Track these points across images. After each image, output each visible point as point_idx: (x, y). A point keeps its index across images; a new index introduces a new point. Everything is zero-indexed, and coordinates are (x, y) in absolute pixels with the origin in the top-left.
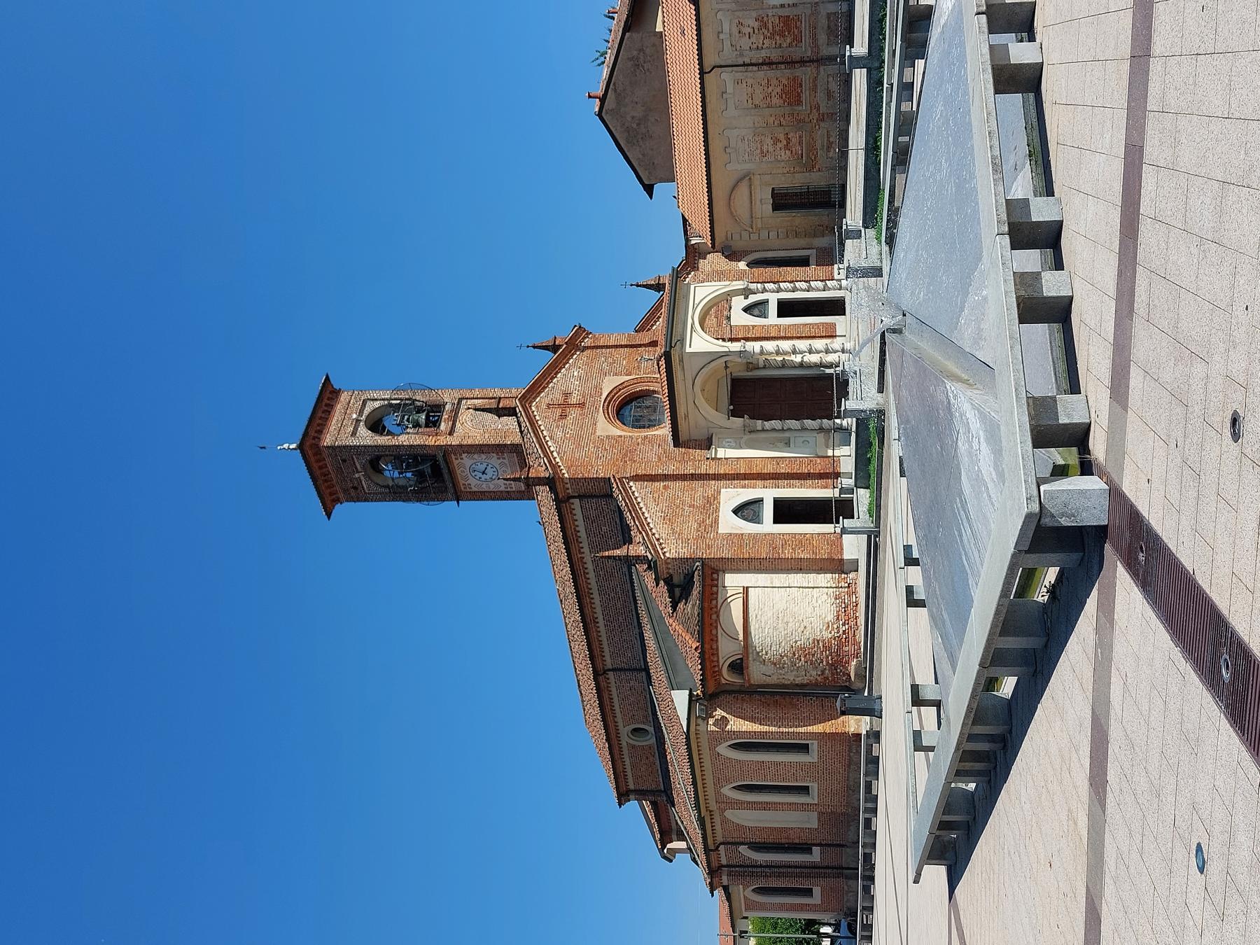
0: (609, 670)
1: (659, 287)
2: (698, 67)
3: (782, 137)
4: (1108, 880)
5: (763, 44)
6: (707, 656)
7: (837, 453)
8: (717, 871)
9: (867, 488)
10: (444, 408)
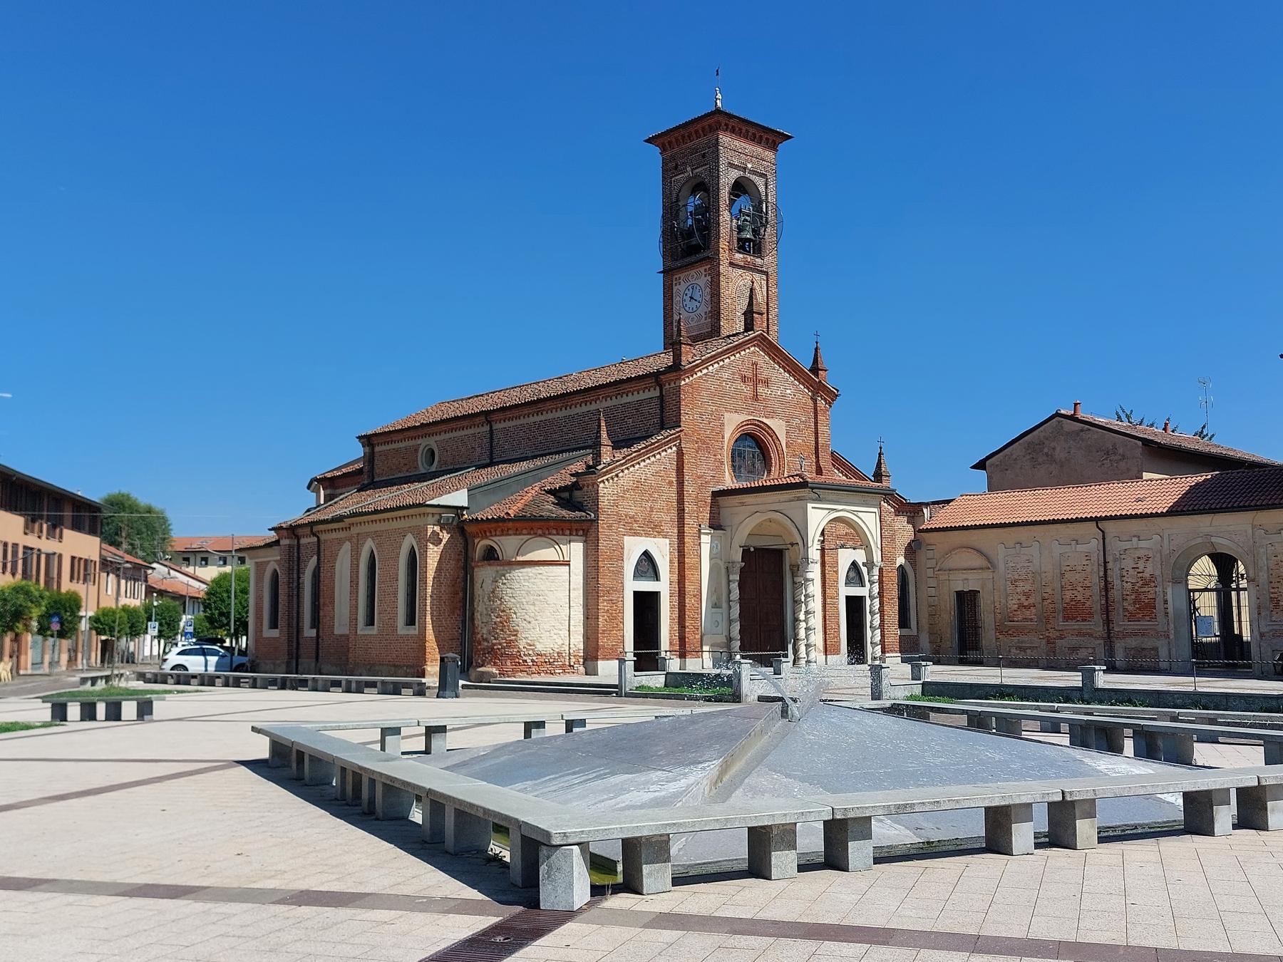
0: (491, 427)
1: (878, 476)
2: (1159, 512)
3: (1031, 601)
4: (209, 905)
5: (1127, 582)
6: (501, 524)
7: (706, 655)
8: (294, 535)
9: (666, 685)
10: (757, 257)
